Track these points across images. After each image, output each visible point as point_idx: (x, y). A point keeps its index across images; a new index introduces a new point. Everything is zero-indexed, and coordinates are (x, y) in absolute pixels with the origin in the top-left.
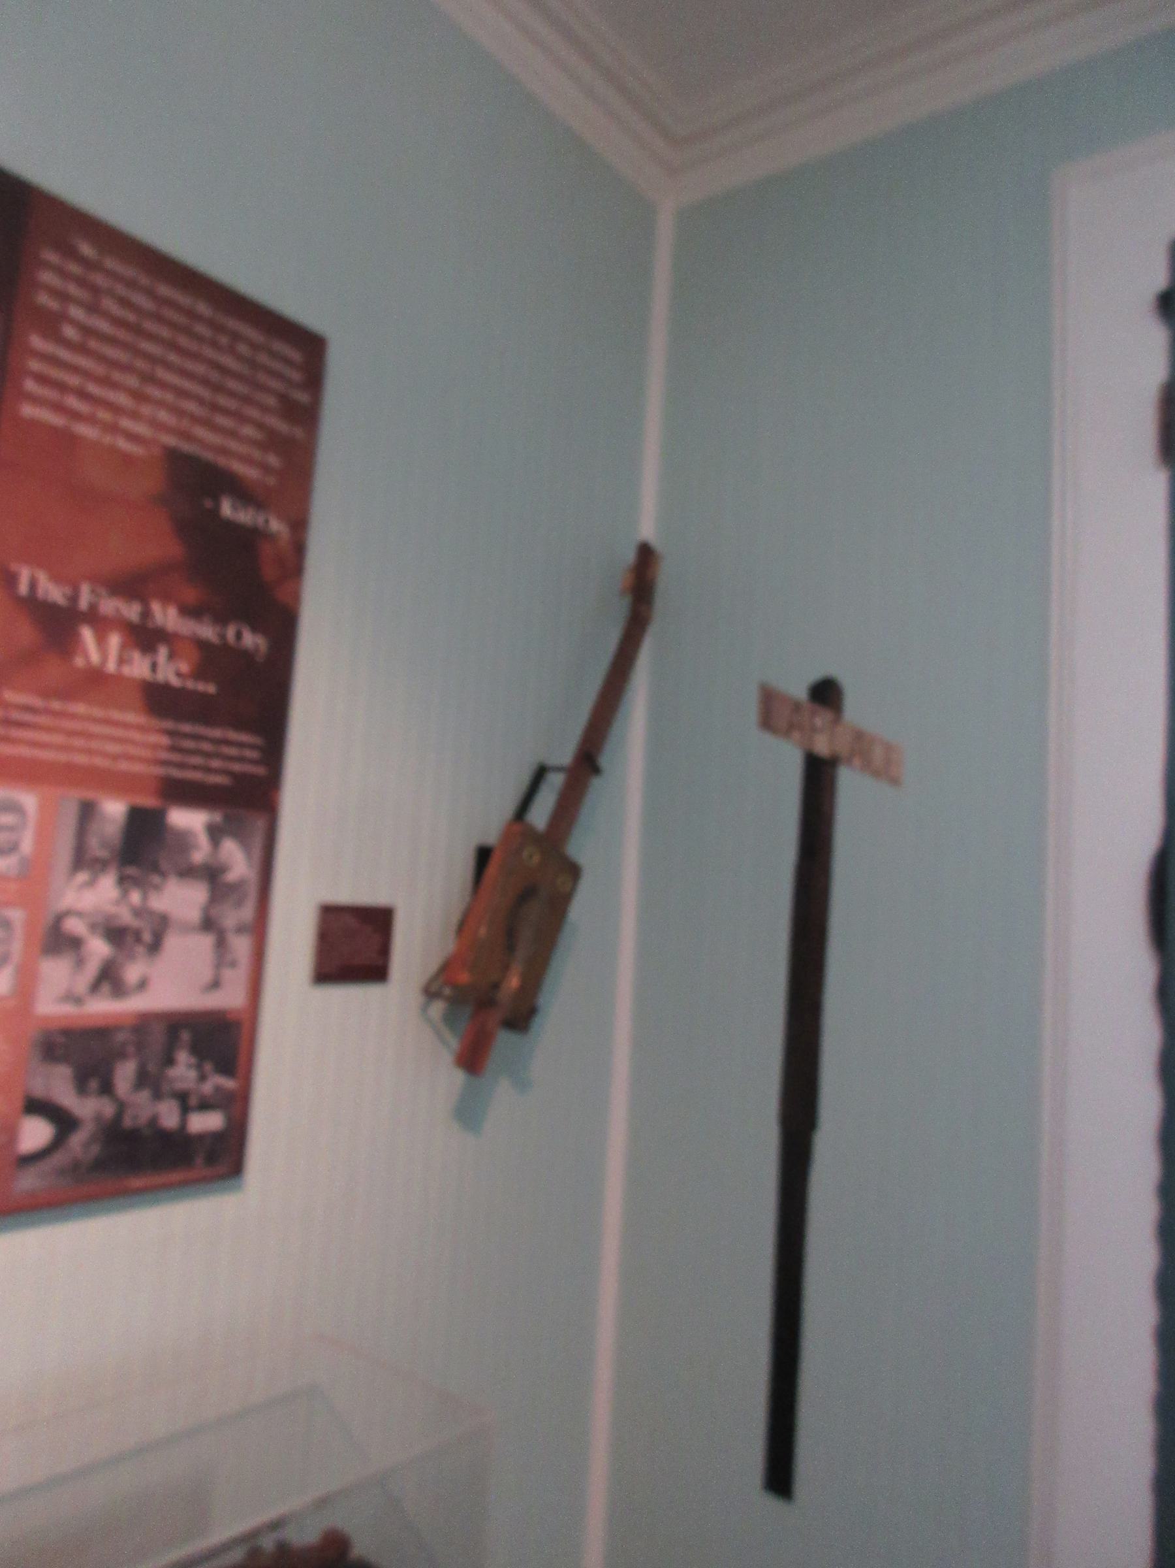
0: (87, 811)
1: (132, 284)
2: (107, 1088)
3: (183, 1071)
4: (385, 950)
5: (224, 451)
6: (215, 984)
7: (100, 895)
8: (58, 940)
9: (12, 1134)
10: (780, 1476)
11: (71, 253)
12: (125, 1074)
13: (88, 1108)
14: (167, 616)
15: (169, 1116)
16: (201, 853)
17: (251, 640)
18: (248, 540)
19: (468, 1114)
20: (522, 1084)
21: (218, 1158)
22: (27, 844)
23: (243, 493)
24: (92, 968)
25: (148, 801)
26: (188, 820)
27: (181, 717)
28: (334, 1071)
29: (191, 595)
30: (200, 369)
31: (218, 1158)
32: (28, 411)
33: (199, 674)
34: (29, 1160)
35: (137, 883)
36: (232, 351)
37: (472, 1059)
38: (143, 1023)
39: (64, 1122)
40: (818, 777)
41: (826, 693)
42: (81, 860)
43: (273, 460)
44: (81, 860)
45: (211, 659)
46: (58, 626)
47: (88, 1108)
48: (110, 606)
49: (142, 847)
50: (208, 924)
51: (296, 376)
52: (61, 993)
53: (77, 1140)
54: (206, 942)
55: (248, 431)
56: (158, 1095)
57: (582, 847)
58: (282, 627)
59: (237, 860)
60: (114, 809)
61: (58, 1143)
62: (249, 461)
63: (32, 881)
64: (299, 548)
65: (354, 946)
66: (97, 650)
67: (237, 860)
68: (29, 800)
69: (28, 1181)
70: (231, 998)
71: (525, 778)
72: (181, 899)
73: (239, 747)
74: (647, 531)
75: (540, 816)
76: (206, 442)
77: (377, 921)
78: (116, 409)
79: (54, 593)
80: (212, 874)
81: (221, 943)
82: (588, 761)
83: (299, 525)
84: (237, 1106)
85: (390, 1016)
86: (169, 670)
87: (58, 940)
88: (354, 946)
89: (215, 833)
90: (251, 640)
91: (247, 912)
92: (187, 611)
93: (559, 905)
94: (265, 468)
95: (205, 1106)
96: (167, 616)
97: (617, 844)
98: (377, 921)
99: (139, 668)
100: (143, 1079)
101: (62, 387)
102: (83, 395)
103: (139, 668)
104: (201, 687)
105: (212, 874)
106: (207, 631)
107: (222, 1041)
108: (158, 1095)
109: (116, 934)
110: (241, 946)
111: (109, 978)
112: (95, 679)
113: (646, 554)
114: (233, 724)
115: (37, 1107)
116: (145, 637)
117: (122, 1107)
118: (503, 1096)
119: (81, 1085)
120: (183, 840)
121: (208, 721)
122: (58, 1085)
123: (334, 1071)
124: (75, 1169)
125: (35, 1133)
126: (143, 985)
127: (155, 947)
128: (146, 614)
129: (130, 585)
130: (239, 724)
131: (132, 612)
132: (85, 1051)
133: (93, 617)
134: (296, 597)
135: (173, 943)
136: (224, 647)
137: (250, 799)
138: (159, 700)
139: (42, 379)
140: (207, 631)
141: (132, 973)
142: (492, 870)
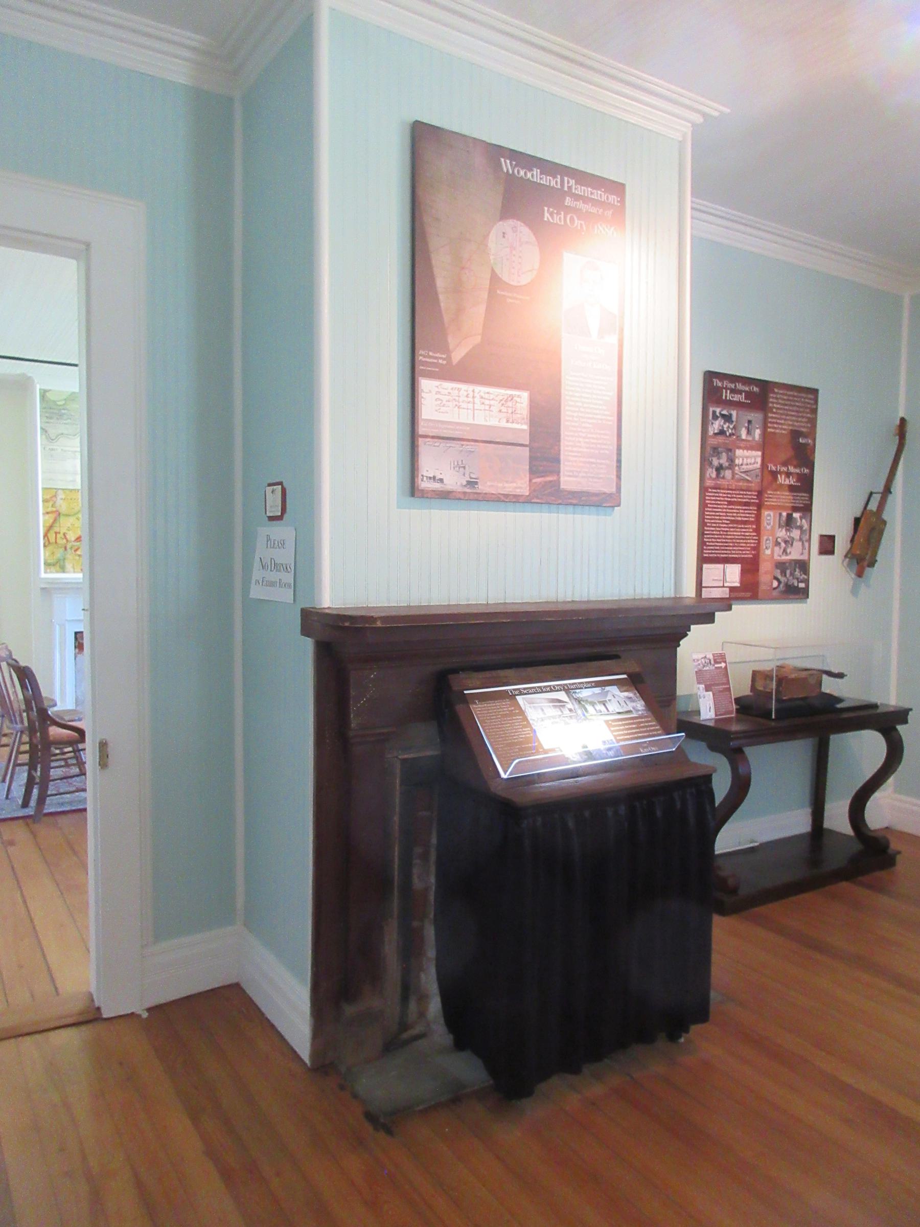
2: (785, 576)
6: (802, 554)
14: (792, 469)
17: (806, 471)
19: (854, 591)
20: (868, 586)
26: (796, 515)
27: (796, 492)
28: (826, 574)
29: (795, 463)
30: (795, 408)
33: (797, 481)
34: (775, 589)
37: (860, 574)
42: (780, 526)
43: (809, 425)
44: (780, 526)
46: (774, 474)
47: (783, 579)
49: (789, 523)
50: (801, 539)
51: (812, 402)
52: (778, 555)
55: (804, 420)
57: (885, 516)
58: (811, 466)
60: (784, 514)
62: (804, 427)
64: (814, 445)
65: (827, 545)
66: (781, 479)
68: (772, 513)
69: (775, 593)
71: (866, 496)
72: (796, 534)
74: (901, 414)
75: (873, 506)
77: (832, 538)
79: (774, 468)
80: (801, 528)
81: (803, 544)
82: (887, 490)
83: (814, 440)
84: (807, 582)
85: (836, 560)
86: (792, 481)
87: (777, 544)
88: (827, 545)
89: (801, 518)
90: (806, 471)
91: (807, 537)
93: (881, 533)
95: (802, 582)
96: (792, 469)
97: (896, 513)
98: (832, 538)
100: (791, 574)
102: (777, 423)
103: (787, 482)
104: (39, 769)
106: (798, 471)
107: (803, 566)
109: (786, 542)
110: (806, 544)
112: (781, 485)
113: (903, 421)
116: (788, 474)
118: (863, 589)
119: (781, 573)
121: (800, 492)
123: (826, 574)
125: (775, 584)
129: (785, 464)
130: (805, 492)
133: (780, 473)
135: (795, 543)
137: (807, 509)
138: (792, 488)
140: (798, 471)
141: (788, 551)
142: (862, 524)
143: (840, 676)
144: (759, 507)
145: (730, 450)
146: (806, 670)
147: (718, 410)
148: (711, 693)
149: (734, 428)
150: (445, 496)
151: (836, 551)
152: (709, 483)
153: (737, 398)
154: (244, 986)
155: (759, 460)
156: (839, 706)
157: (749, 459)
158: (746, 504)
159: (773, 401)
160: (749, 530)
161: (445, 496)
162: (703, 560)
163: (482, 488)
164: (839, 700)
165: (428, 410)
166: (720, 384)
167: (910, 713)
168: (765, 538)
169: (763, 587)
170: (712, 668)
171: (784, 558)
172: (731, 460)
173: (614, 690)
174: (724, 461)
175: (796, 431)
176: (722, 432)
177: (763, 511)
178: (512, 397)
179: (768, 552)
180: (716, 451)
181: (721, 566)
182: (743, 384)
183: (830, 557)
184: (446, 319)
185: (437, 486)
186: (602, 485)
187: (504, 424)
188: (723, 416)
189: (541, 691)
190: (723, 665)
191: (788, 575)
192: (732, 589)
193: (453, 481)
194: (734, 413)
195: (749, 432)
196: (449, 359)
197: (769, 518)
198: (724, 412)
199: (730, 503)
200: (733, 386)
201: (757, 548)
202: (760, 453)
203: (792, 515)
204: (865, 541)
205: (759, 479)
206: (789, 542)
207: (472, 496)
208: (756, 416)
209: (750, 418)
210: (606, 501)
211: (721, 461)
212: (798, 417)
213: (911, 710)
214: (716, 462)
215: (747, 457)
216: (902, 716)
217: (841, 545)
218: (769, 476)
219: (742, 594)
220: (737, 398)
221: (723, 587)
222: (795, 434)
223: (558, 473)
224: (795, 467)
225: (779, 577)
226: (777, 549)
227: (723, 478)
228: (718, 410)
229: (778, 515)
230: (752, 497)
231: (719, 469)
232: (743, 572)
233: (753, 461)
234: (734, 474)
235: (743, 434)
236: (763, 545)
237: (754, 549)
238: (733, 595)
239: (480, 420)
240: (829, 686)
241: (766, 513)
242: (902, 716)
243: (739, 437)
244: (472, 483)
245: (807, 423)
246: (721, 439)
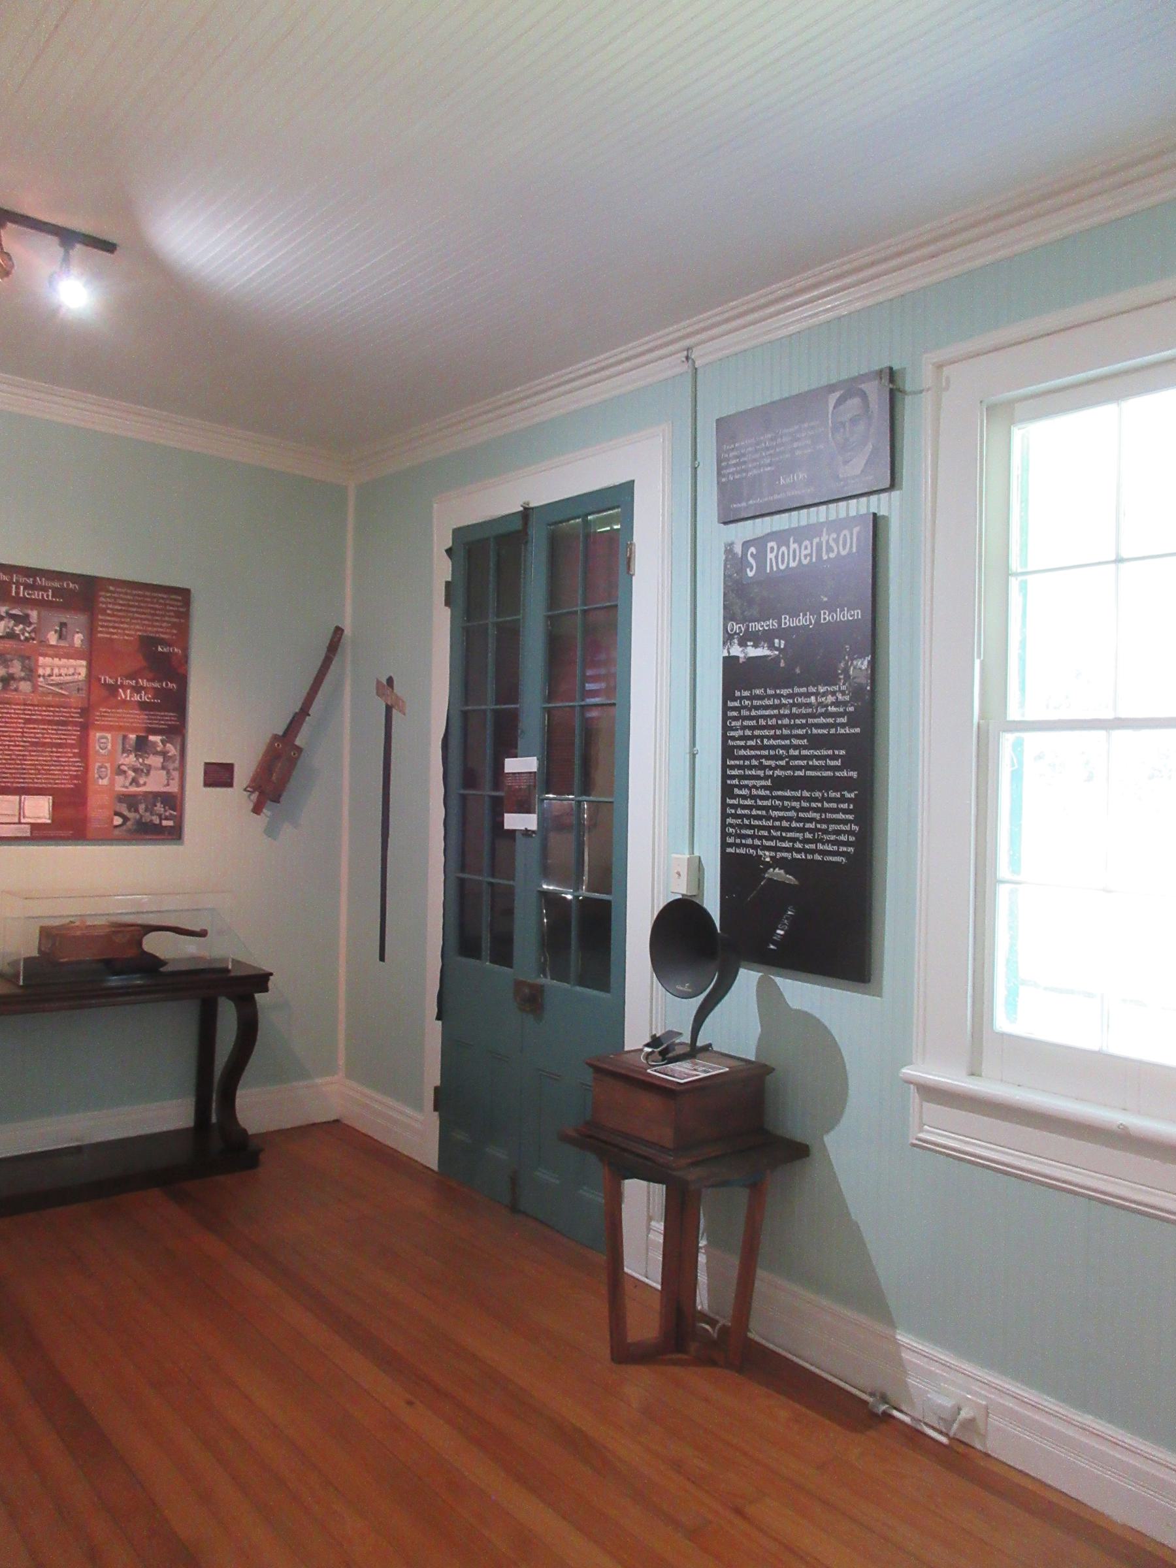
0: (125, 737)
1: (126, 594)
2: (137, 811)
3: (159, 808)
4: (232, 778)
5: (157, 632)
7: (131, 759)
8: (120, 772)
9: (112, 820)
10: (382, 958)
11: (108, 591)
12: (142, 807)
14: (143, 682)
15: (156, 820)
21: (175, 834)
22: (109, 747)
23: (163, 642)
24: (130, 779)
32: (99, 635)
34: (116, 827)
35: (141, 756)
36: (157, 603)
39: (125, 819)
40: (389, 709)
41: (390, 681)
42: (124, 750)
44: (124, 750)
45: (157, 692)
46: (113, 690)
49: (142, 747)
52: (121, 785)
53: (129, 823)
54: (164, 772)
55: (164, 624)
56: (152, 814)
59: (172, 750)
60: (133, 736)
63: (111, 755)
65: (219, 775)
67: (172, 750)
68: (109, 736)
69: (117, 832)
70: (174, 788)
72: (155, 761)
73: (170, 717)
76: (151, 632)
77: (229, 768)
78: (124, 629)
79: (110, 681)
80: (164, 754)
81: (168, 772)
85: (236, 797)
87: (120, 772)
88: (219, 775)
91: (177, 764)
92: (148, 680)
94: (173, 634)
95: (166, 819)
96: (143, 682)
98: (229, 768)
99: (137, 698)
100: (146, 810)
101: (107, 627)
103: (137, 698)
105: (164, 754)
106: (157, 685)
107: (173, 802)
108: (152, 814)
109: (135, 770)
110: (176, 774)
111: (134, 781)
112: (124, 702)
114: (170, 710)
115: (117, 814)
116: (137, 689)
117: (141, 817)
120: (154, 744)
124: (129, 831)
125: (118, 821)
126: (145, 784)
128: (137, 683)
131: (133, 683)
132: (131, 801)
133: (122, 686)
135: (152, 772)
137: (177, 731)
138: (143, 706)
139: (102, 626)
141: (141, 782)
143: (203, 934)
145: (29, 658)
146: (132, 925)
149: (33, 631)
153: (37, 595)
154: (108, 254)
155: (83, 672)
159: (103, 599)
160: (69, 756)
164: (163, 963)
167: (271, 978)
168: (98, 764)
172: (31, 673)
174: (16, 668)
175: (148, 637)
177: (92, 733)
179: (105, 782)
182: (47, 579)
183: (229, 790)
191: (141, 811)
192: (34, 826)
194: (34, 615)
197: (103, 742)
201: (83, 777)
202: (84, 663)
204: (275, 780)
205: (83, 694)
208: (76, 620)
209: (65, 620)
211: (11, 671)
212: (153, 621)
213: (271, 974)
215: (59, 667)
217: (243, 775)
219: (52, 833)
220: (37, 595)
221: (20, 823)
222: (148, 644)
225: (126, 813)
226: (120, 780)
227: (16, 690)
229: (120, 741)
232: (55, 806)
233: (71, 671)
235: (53, 638)
236: (94, 772)
238: (36, 833)
241: (98, 734)
242: (261, 981)
243: (44, 642)
245: (171, 628)
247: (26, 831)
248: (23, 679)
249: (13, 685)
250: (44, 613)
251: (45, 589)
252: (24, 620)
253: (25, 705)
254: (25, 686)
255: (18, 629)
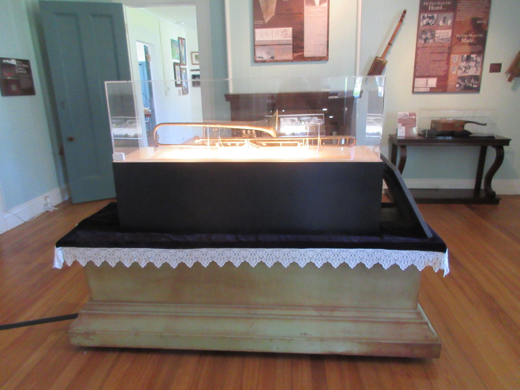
3: (472, 81)
6: (476, 72)
8: (460, 68)
10: (405, 12)
12: (466, 81)
13: (463, 84)
15: (471, 85)
16: (475, 59)
17: (481, 35)
18: (481, 24)
21: (477, 90)
25: (469, 54)
26: (473, 56)
31: (477, 90)
38: (468, 76)
39: (460, 85)
42: (462, 61)
44: (462, 61)
46: (460, 39)
48: (465, 36)
52: (460, 73)
58: (485, 33)
60: (465, 56)
61: (460, 87)
65: (496, 68)
66: (463, 41)
67: (479, 59)
68: (457, 56)
69: (457, 90)
70: (478, 74)
72: (472, 64)
79: (459, 36)
80: (476, 61)
81: (477, 68)
85: (502, 76)
86: (471, 41)
87: (460, 68)
88: (496, 68)
89: (476, 57)
90: (481, 35)
100: (468, 81)
103: (468, 41)
107: (477, 78)
109: (465, 67)
110: (479, 69)
111: (465, 72)
114: (479, 45)
115: (458, 83)
116: (468, 38)
119: (462, 81)
120: (473, 58)
122: (460, 81)
123: (488, 79)
127: (470, 68)
131: (467, 36)
132: (463, 78)
134: (487, 29)
135: (471, 68)
136: (477, 37)
137: (481, 52)
138: (470, 44)
140: (476, 36)
141: (467, 71)
143: (485, 125)
144: (449, 54)
147: (426, 15)
148: (404, 127)
149: (435, 21)
150: (264, 62)
151: (502, 70)
152: (419, 46)
153: (437, 8)
156: (471, 135)
157: (444, 34)
158: (443, 53)
160: (444, 64)
161: (264, 62)
162: (415, 77)
163: (276, 59)
164: (471, 134)
165: (258, 38)
166: (427, 4)
169: (449, 87)
170: (407, 118)
171: (464, 75)
172: (433, 36)
173: (316, 118)
174: (429, 35)
176: (428, 24)
178: (286, 30)
180: (424, 32)
181: (425, 79)
184: (263, 10)
185: (261, 59)
186: (321, 53)
187: (283, 39)
188: (428, 17)
189: (288, 117)
190: (414, 117)
193: (266, 57)
194: (435, 16)
195: (444, 22)
196: (264, 22)
197: (455, 58)
198: (430, 15)
199: (431, 53)
200: (435, 4)
201: (447, 71)
202: (451, 31)
203: (470, 56)
206: (468, 68)
207: (273, 61)
210: (323, 59)
214: (424, 37)
215: (443, 33)
216: (506, 142)
217: (505, 68)
218: (455, 40)
220: (437, 8)
222: (474, 21)
223: (303, 51)
224: (473, 34)
227: (428, 43)
228: (426, 15)
230: (447, 50)
231: (425, 40)
232: (438, 81)
234: (434, 41)
235: (441, 23)
237: (445, 71)
239: (275, 39)
240: (468, 127)
241: (453, 56)
242: (506, 142)
244: (272, 58)
246: (427, 27)
247: (428, 90)
248: (430, 39)
249: (427, 41)
250: (440, 14)
251: (439, 6)
252: (432, 18)
253: (431, 47)
254: (431, 41)
255: (430, 22)
